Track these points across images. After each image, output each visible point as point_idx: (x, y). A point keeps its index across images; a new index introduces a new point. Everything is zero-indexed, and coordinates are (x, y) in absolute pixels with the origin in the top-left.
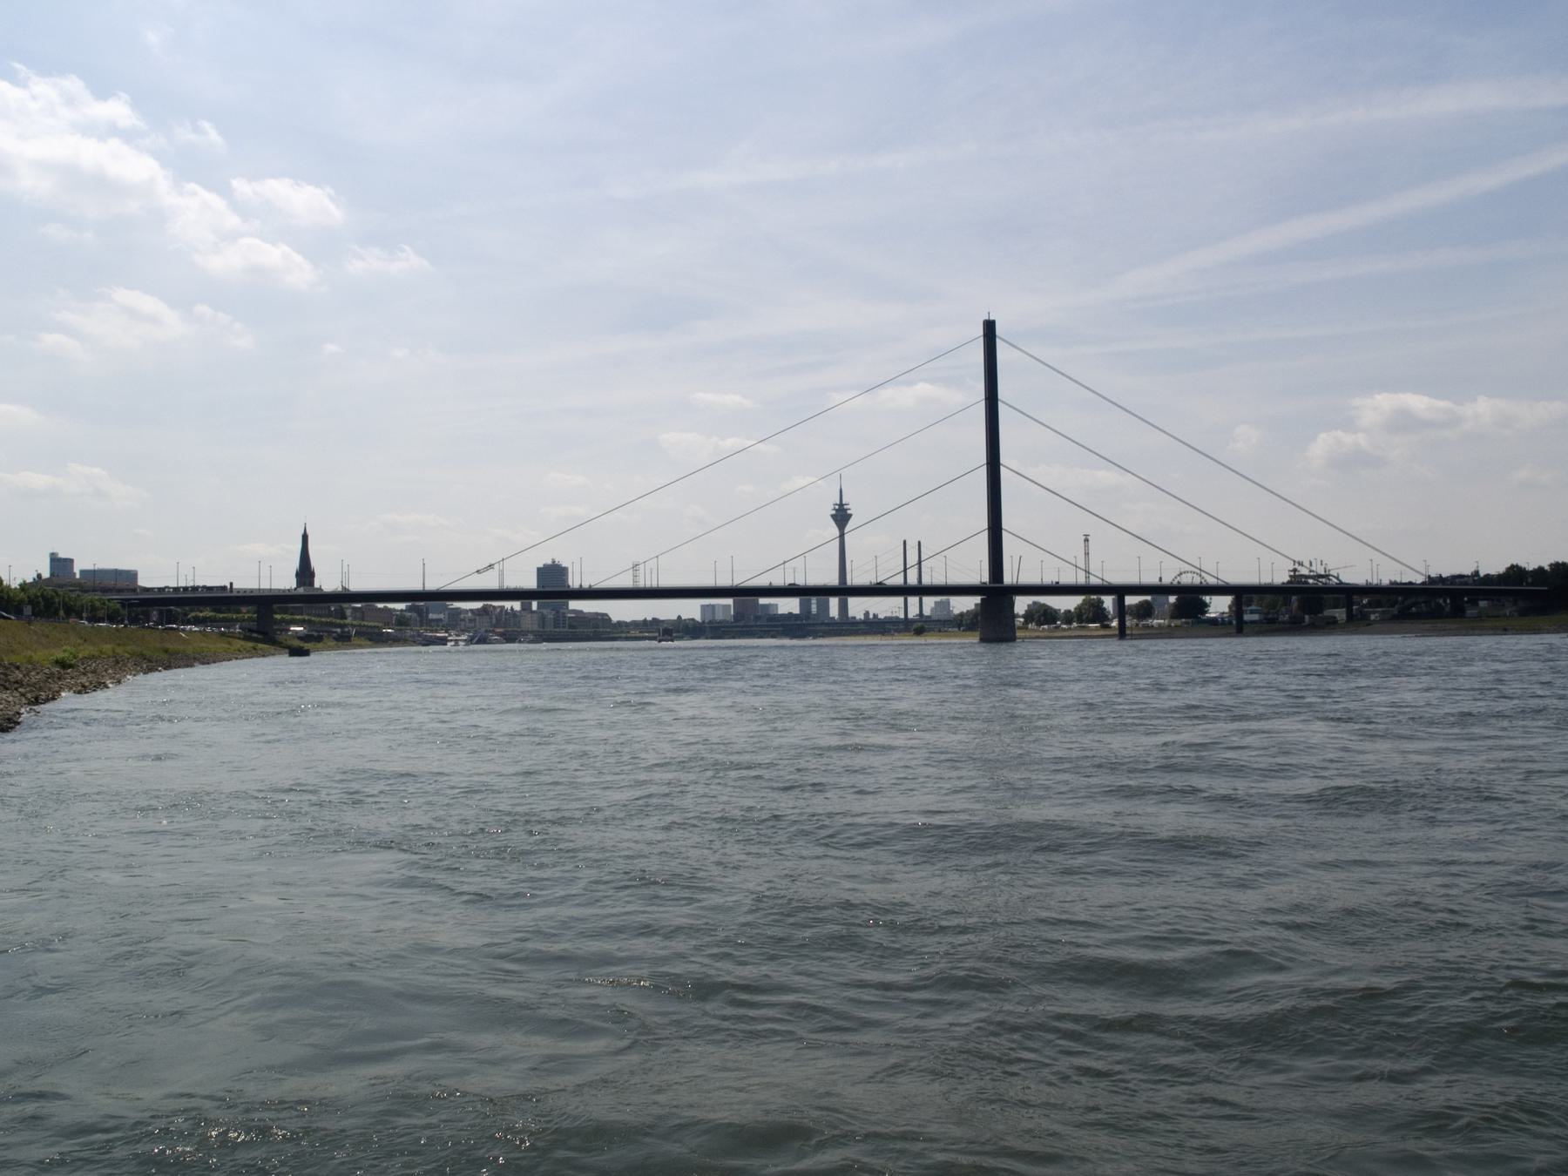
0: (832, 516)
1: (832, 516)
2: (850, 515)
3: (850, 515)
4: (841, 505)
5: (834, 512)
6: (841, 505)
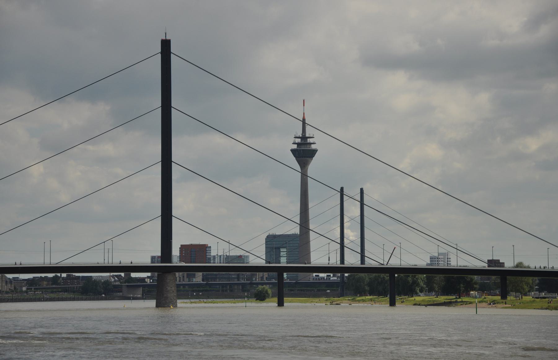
4: (304, 138)
5: (295, 147)
6: (304, 138)
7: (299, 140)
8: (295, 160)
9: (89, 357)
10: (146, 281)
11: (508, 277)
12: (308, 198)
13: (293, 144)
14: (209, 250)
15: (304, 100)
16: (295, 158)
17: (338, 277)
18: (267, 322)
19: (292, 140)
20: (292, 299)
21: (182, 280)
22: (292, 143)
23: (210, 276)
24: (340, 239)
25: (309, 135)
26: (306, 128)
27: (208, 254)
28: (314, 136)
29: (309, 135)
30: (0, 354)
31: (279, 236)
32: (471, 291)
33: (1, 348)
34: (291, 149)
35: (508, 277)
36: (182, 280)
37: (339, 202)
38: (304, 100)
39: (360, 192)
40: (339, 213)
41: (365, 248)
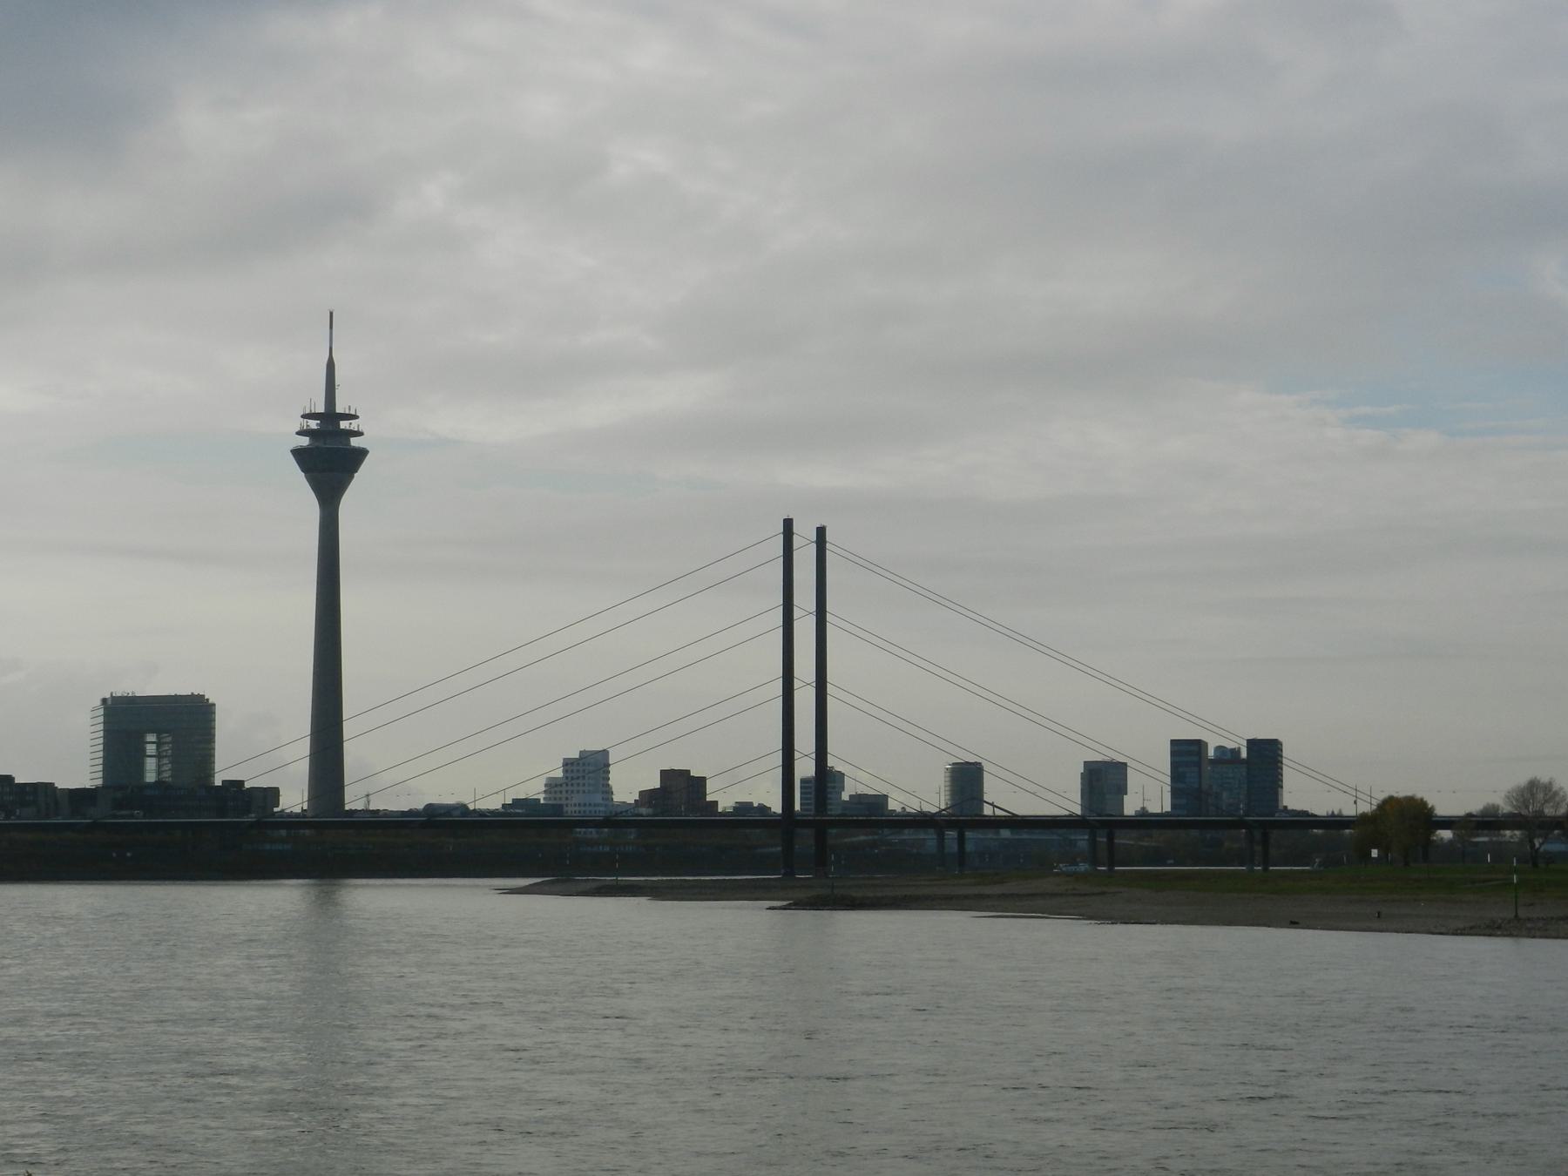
0: (298, 453)
1: (298, 453)
2: (361, 454)
3: (361, 454)
5: (305, 441)
7: (313, 424)
8: (305, 479)
9: (774, 1027)
12: (792, 564)
13: (298, 433)
15: (331, 314)
16: (303, 474)
18: (62, 1143)
19: (298, 423)
21: (810, 785)
22: (298, 429)
25: (350, 409)
26: (337, 391)
29: (350, 409)
30: (3, 1123)
32: (1450, 841)
33: (3, 1099)
34: (292, 448)
36: (810, 785)
38: (331, 314)
40: (796, 624)
41: (796, 748)
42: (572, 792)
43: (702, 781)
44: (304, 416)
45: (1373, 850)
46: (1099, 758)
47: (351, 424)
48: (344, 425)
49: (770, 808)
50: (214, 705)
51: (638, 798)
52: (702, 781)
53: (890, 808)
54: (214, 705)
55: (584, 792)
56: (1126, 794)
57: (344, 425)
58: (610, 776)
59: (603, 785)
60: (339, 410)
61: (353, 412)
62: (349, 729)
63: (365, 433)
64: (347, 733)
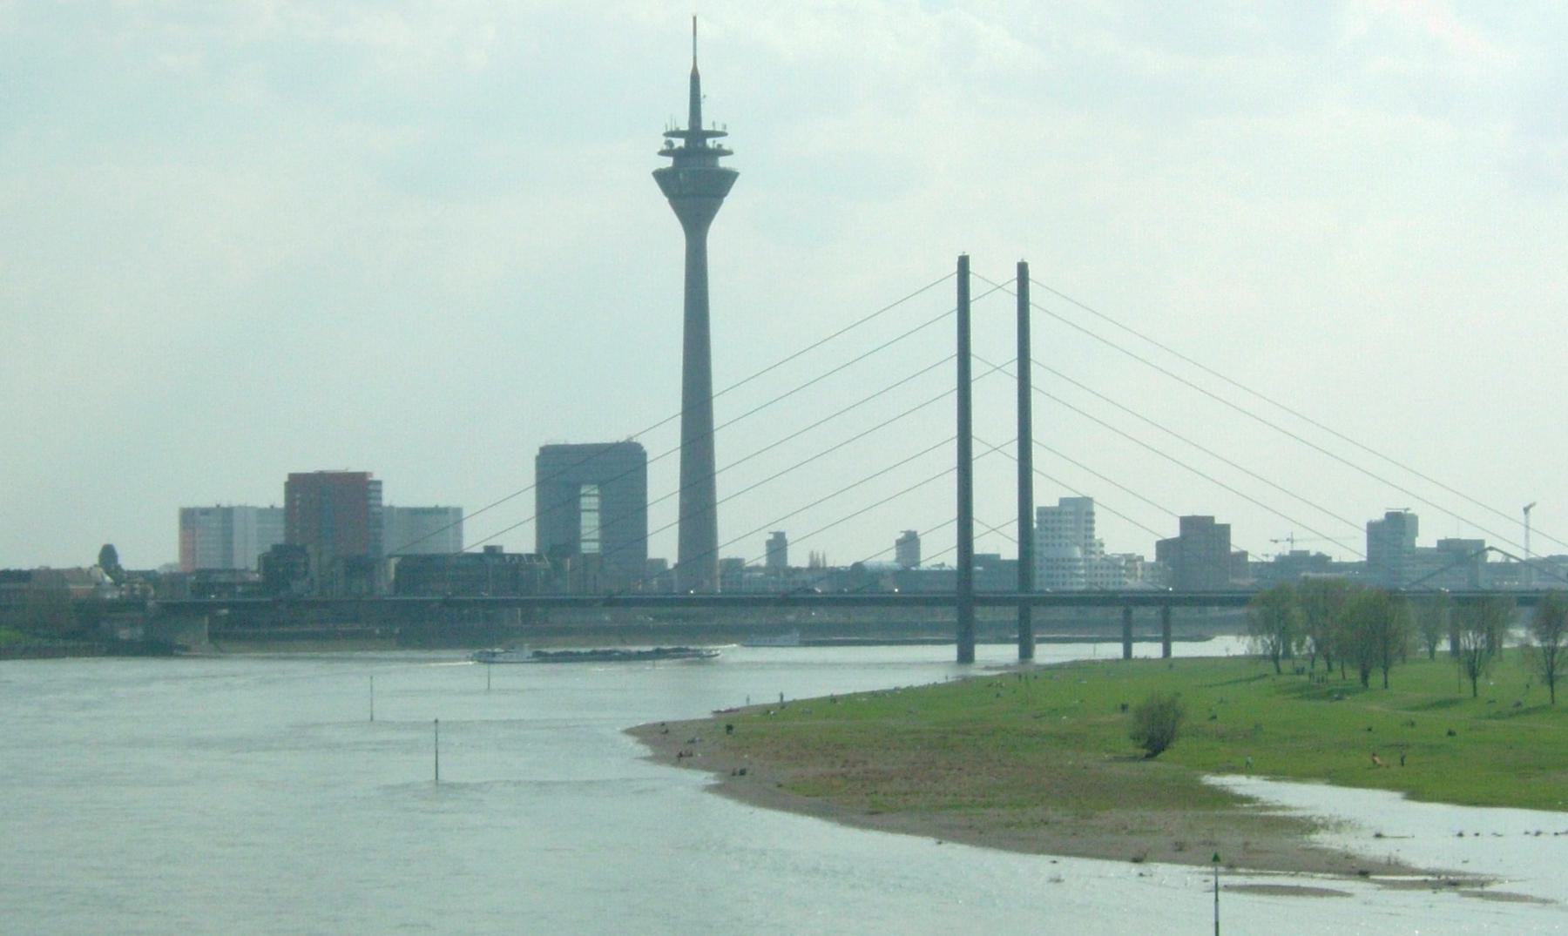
0: (661, 176)
1: (661, 176)
2: (729, 177)
3: (729, 177)
4: (695, 134)
5: (668, 162)
6: (695, 134)
7: (679, 143)
10: (1517, 564)
11: (1034, 610)
14: (374, 491)
15: (695, 19)
17: (1511, 639)
20: (425, 596)
23: (71, 644)
24: (678, 498)
27: (372, 502)
28: (727, 131)
31: (610, 448)
34: (655, 168)
35: (1034, 610)
37: (1015, 434)
38: (695, 19)
39: (955, 268)
42: (1047, 545)
43: (1225, 529)
44: (667, 134)
45: (1489, 560)
46: (1073, 495)
47: (714, 142)
48: (710, 142)
49: (1330, 558)
50: (379, 483)
51: (1250, 559)
52: (1225, 529)
53: (1233, 550)
54: (379, 483)
55: (1054, 545)
56: (1212, 518)
57: (710, 142)
58: (1095, 525)
59: (1086, 537)
60: (706, 126)
61: (719, 128)
62: (1016, 399)
63: (734, 151)
64: (720, 494)
